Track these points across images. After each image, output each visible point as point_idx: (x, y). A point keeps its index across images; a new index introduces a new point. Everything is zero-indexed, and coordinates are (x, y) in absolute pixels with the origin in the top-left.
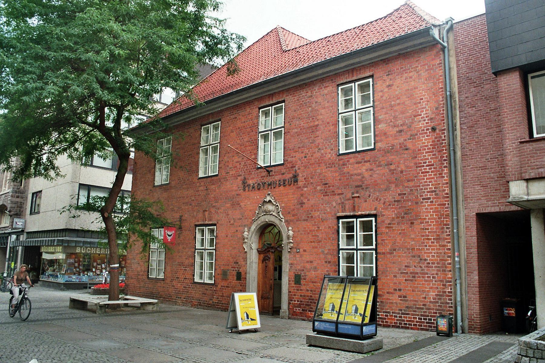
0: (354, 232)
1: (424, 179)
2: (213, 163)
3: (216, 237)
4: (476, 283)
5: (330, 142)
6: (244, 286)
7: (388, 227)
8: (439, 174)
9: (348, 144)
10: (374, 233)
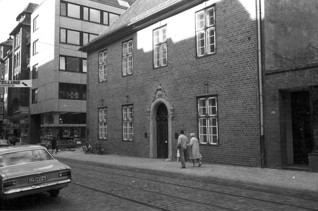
0: (215, 106)
1: (243, 71)
5: (192, 50)
7: (224, 103)
8: (252, 68)
9: (203, 52)
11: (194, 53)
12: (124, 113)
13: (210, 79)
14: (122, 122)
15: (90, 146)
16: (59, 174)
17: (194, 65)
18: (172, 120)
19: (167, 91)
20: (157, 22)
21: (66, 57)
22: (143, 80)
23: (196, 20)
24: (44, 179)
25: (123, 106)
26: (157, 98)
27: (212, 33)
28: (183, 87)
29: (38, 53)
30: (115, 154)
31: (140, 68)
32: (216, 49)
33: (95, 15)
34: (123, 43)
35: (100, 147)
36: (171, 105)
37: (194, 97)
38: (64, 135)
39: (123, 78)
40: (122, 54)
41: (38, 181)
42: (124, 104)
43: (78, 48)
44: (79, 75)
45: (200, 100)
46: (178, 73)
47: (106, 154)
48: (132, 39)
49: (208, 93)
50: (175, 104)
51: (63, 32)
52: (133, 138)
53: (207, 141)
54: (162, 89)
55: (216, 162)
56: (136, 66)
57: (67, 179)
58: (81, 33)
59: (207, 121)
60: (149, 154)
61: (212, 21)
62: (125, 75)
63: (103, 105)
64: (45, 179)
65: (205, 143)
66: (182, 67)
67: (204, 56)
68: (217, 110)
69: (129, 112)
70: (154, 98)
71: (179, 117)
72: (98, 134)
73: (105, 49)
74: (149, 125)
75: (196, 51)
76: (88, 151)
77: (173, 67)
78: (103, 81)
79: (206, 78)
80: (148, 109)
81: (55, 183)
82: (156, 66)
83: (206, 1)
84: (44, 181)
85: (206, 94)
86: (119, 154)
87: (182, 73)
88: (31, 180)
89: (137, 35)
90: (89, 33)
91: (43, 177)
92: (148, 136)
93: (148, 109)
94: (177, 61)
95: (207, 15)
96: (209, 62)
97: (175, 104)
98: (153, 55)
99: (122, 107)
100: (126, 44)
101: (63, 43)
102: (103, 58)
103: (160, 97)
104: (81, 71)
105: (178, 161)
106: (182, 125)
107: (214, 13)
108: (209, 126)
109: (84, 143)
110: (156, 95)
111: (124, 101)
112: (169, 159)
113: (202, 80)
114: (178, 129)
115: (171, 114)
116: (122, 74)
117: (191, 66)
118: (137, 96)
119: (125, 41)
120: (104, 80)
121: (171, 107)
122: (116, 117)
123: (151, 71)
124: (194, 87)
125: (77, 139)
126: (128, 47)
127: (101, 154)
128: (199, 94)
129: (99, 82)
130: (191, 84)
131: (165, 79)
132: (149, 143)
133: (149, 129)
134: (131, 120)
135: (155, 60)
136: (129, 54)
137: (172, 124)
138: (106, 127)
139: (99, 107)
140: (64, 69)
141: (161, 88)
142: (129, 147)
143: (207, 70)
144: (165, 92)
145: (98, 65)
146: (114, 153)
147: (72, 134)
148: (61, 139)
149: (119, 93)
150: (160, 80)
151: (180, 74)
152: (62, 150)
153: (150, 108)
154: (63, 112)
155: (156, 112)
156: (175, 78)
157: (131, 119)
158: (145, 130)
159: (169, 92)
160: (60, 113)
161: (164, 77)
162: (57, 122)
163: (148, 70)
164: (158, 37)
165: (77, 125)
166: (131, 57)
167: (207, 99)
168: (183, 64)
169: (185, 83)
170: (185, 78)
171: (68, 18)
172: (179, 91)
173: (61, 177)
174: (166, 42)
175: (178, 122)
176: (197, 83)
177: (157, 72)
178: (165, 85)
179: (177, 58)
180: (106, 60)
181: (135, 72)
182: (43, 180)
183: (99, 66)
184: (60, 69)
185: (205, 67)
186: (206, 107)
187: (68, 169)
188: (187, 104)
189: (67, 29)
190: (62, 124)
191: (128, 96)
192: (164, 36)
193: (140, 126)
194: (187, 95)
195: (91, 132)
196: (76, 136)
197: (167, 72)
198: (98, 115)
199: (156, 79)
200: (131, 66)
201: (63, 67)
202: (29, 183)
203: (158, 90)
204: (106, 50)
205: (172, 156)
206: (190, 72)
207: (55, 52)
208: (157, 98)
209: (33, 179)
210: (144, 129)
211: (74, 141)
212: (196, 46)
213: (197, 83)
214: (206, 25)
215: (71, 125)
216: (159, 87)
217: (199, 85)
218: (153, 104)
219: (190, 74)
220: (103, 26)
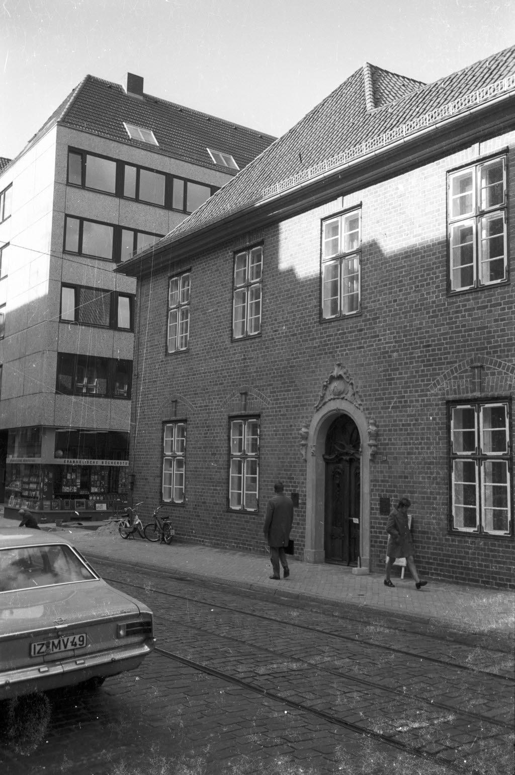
2: (184, 332)
3: (260, 435)
4: (462, 476)
6: (376, 542)
8: (490, 343)
10: (507, 429)
11: (442, 281)
12: (234, 437)
13: (488, 353)
14: (229, 461)
15: (137, 521)
16: (119, 628)
17: (442, 315)
18: (372, 460)
19: (360, 383)
20: (334, 198)
21: (77, 288)
22: (291, 351)
23: (451, 191)
24: (73, 643)
25: (231, 418)
26: (330, 400)
27: (495, 227)
28: (406, 373)
29: (6, 276)
30: (207, 546)
31: (283, 318)
32: (508, 271)
33: (154, 187)
34: (236, 253)
35: (166, 524)
36: (371, 421)
37: (440, 399)
38: (66, 485)
39: (234, 344)
40: (233, 282)
41: (55, 650)
42: (235, 413)
43: (114, 266)
44: (107, 334)
45: (457, 411)
46: (391, 333)
47: (181, 542)
48: (261, 243)
49: (482, 390)
50: (382, 417)
51: (73, 224)
52: (258, 505)
53: (478, 523)
54: (344, 376)
55: (505, 585)
56: (272, 313)
57: (140, 644)
58: (118, 231)
59: (477, 468)
60: (302, 549)
61: (495, 196)
62: (238, 336)
63: (175, 415)
64: (78, 646)
65: (471, 530)
66: (405, 317)
67: (473, 288)
68: (508, 439)
69: (247, 437)
70: (322, 400)
71: (393, 453)
72: (161, 489)
73: (184, 268)
74: (303, 472)
75: (448, 275)
76: (132, 533)
77: (378, 318)
78: (178, 353)
79: (478, 349)
80: (304, 430)
81: (106, 659)
82: (328, 315)
83: (482, 141)
84: (73, 650)
85: (477, 394)
86: (218, 544)
87: (405, 336)
88: (38, 648)
89: (278, 230)
90: (136, 231)
91: (71, 639)
92: (300, 501)
93: (304, 430)
94: (390, 302)
95: (482, 178)
96: (486, 307)
97: (382, 417)
98: (320, 285)
99: (229, 422)
100: (245, 255)
101: (71, 253)
102: (178, 293)
103: (338, 398)
104: (113, 325)
105: (402, 577)
106: (400, 477)
107: (504, 173)
108: (484, 487)
109: (116, 510)
110: (328, 393)
111: (236, 405)
112: (363, 568)
113: (464, 356)
114: (390, 486)
115: (370, 446)
116: (232, 334)
117: (432, 317)
118: (271, 393)
119: (241, 247)
120: (181, 349)
121: (370, 427)
122: (212, 447)
123: (313, 327)
124: (438, 374)
125: (98, 498)
126: (250, 265)
127: (169, 544)
128: (455, 394)
129: (167, 354)
130: (431, 365)
131: (354, 349)
132: (304, 520)
133: (303, 483)
134: (252, 457)
135: (327, 299)
136: (252, 282)
137: (371, 472)
138: (184, 472)
139: (164, 419)
140: (72, 317)
141: (341, 373)
142: (245, 529)
143: (479, 329)
144: (352, 384)
145: (166, 308)
146: (201, 543)
147: (86, 485)
148: (56, 497)
149: (221, 384)
150: (340, 351)
151: (400, 337)
152: (61, 526)
153: (307, 427)
154: (63, 428)
155: (323, 441)
156: (384, 348)
157: (254, 454)
158: (292, 486)
159: (365, 387)
160: (58, 429)
161: (351, 345)
162: (48, 454)
163: (303, 325)
164: (337, 240)
165: (99, 462)
166: (187, 311)
167: (479, 407)
168: (409, 312)
169: (411, 363)
170: (413, 349)
171: (86, 192)
172: (396, 384)
173: (123, 637)
174: (359, 252)
175: (390, 468)
176: (448, 363)
177: (331, 331)
178: (352, 367)
179: (391, 293)
180: (186, 296)
181: (268, 329)
182: (73, 647)
183: (168, 313)
184: (62, 318)
185: (476, 319)
186: (476, 430)
187: (143, 614)
188: (417, 420)
189: (82, 220)
190: (60, 458)
191: (246, 394)
192: (353, 237)
193: (279, 474)
194: (419, 396)
195: (140, 483)
196: (94, 490)
197: (361, 330)
198: (163, 439)
199: (329, 349)
200: (257, 313)
201: (69, 312)
202: (30, 656)
203: (332, 379)
204: (189, 270)
205: (371, 561)
206: (427, 332)
207: (50, 276)
208: (330, 400)
209: (43, 644)
210: (291, 482)
211: (90, 504)
212: (448, 261)
213: (448, 363)
214: (479, 205)
215: (84, 462)
216: (336, 372)
217: (456, 368)
218: (317, 419)
219: (430, 337)
220: (171, 213)
